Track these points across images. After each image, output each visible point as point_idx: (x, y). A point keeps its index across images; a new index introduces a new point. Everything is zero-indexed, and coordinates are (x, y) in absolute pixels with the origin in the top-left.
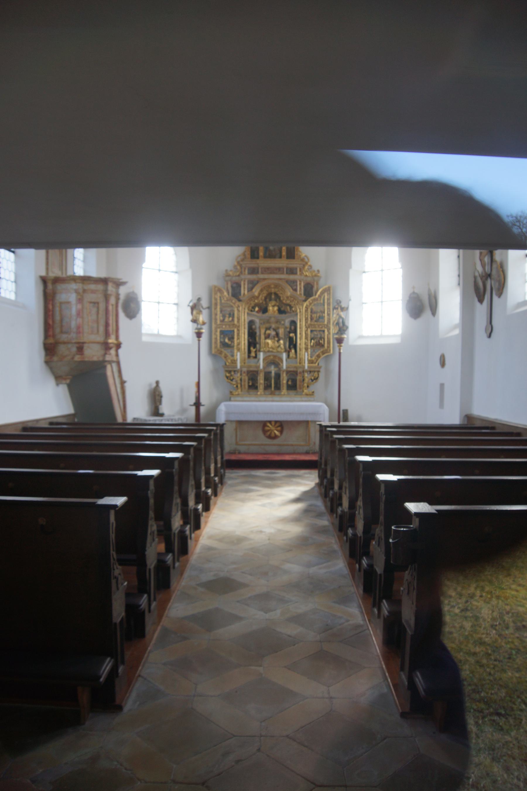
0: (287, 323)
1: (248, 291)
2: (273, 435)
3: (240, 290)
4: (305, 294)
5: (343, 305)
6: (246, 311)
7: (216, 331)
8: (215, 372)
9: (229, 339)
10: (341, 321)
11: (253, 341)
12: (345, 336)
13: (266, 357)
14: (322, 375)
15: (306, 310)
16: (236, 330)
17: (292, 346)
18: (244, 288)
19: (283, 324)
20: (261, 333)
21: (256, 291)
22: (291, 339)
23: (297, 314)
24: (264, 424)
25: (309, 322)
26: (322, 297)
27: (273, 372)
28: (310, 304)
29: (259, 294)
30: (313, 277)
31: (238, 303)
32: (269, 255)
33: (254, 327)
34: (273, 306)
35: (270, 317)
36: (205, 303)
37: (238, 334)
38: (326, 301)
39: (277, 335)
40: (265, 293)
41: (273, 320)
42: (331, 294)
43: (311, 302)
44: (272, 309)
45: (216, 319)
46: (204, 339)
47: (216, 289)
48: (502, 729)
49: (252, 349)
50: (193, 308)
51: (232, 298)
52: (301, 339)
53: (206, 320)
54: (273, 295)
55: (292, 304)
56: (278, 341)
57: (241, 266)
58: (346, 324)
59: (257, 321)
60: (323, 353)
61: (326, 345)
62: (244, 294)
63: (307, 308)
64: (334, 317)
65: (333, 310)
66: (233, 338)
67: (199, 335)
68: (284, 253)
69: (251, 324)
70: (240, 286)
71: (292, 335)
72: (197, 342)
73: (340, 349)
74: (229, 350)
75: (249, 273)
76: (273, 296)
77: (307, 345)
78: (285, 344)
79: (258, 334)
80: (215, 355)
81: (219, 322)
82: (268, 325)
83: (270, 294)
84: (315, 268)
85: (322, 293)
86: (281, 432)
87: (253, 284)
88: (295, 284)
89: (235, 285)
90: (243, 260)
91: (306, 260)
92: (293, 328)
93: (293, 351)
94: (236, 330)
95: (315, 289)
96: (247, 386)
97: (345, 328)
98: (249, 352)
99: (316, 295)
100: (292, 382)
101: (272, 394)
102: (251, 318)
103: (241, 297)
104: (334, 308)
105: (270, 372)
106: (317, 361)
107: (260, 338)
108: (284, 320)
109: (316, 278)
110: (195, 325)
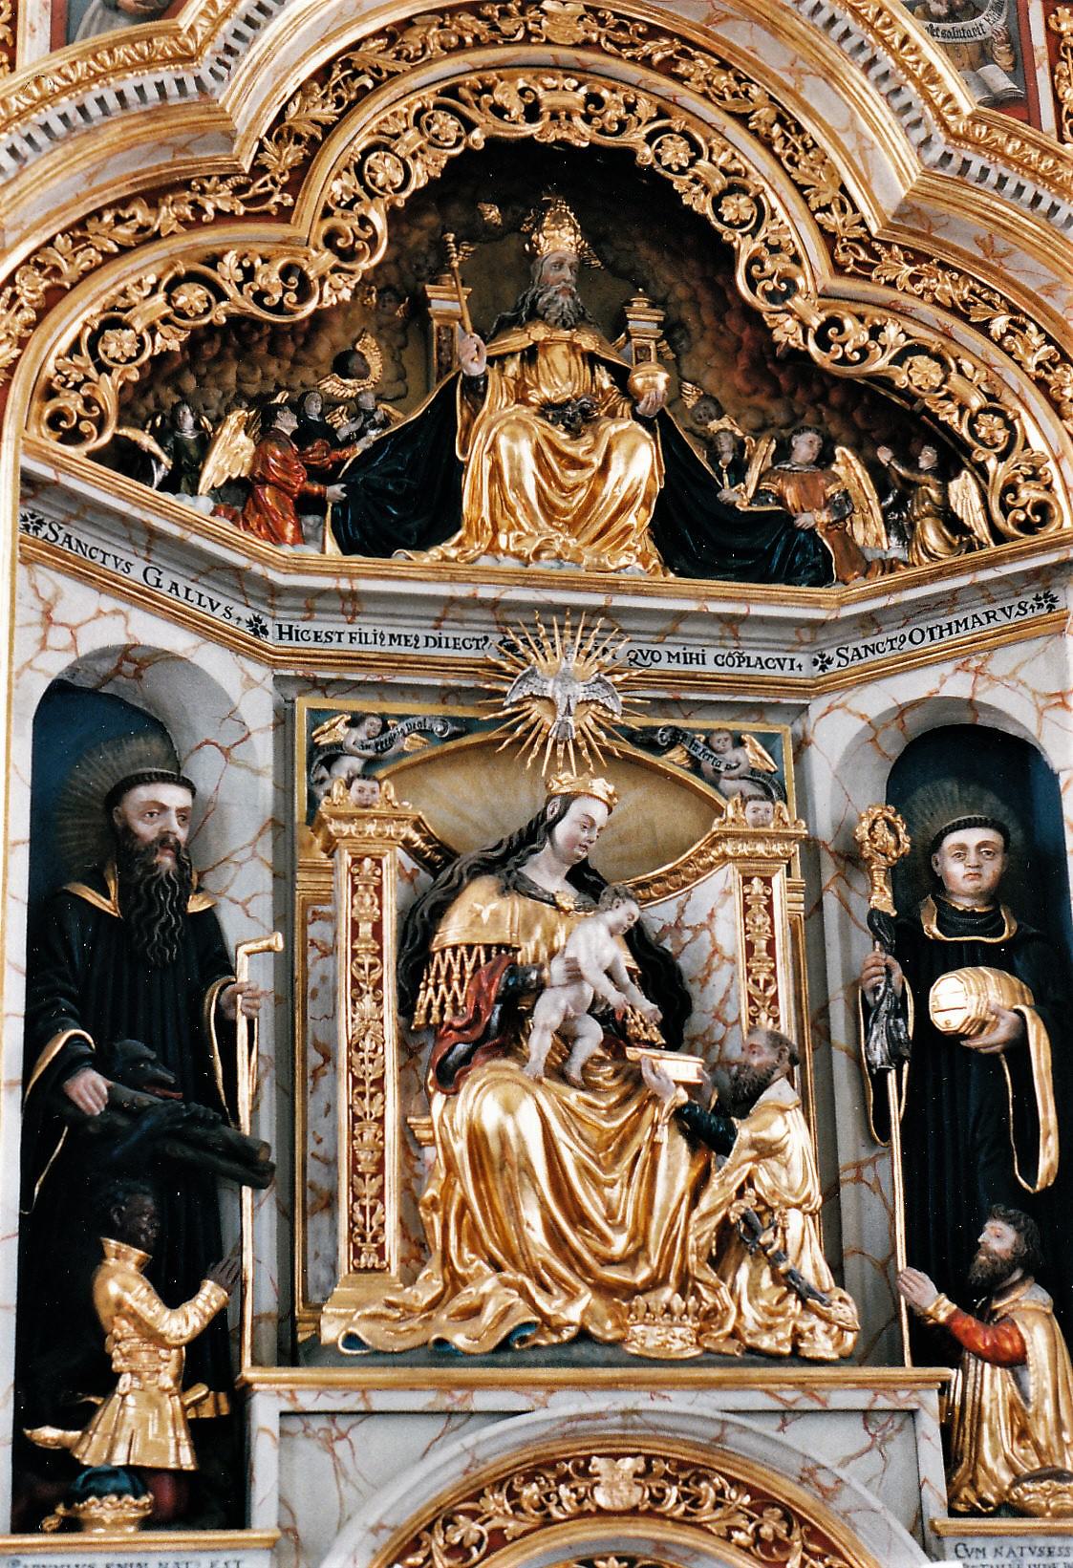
41: (566, 684)
44: (561, 473)
49: (122, 1281)
56: (708, 1128)
59: (233, 692)
82: (468, 803)
102: (97, 624)
107: (296, 1066)
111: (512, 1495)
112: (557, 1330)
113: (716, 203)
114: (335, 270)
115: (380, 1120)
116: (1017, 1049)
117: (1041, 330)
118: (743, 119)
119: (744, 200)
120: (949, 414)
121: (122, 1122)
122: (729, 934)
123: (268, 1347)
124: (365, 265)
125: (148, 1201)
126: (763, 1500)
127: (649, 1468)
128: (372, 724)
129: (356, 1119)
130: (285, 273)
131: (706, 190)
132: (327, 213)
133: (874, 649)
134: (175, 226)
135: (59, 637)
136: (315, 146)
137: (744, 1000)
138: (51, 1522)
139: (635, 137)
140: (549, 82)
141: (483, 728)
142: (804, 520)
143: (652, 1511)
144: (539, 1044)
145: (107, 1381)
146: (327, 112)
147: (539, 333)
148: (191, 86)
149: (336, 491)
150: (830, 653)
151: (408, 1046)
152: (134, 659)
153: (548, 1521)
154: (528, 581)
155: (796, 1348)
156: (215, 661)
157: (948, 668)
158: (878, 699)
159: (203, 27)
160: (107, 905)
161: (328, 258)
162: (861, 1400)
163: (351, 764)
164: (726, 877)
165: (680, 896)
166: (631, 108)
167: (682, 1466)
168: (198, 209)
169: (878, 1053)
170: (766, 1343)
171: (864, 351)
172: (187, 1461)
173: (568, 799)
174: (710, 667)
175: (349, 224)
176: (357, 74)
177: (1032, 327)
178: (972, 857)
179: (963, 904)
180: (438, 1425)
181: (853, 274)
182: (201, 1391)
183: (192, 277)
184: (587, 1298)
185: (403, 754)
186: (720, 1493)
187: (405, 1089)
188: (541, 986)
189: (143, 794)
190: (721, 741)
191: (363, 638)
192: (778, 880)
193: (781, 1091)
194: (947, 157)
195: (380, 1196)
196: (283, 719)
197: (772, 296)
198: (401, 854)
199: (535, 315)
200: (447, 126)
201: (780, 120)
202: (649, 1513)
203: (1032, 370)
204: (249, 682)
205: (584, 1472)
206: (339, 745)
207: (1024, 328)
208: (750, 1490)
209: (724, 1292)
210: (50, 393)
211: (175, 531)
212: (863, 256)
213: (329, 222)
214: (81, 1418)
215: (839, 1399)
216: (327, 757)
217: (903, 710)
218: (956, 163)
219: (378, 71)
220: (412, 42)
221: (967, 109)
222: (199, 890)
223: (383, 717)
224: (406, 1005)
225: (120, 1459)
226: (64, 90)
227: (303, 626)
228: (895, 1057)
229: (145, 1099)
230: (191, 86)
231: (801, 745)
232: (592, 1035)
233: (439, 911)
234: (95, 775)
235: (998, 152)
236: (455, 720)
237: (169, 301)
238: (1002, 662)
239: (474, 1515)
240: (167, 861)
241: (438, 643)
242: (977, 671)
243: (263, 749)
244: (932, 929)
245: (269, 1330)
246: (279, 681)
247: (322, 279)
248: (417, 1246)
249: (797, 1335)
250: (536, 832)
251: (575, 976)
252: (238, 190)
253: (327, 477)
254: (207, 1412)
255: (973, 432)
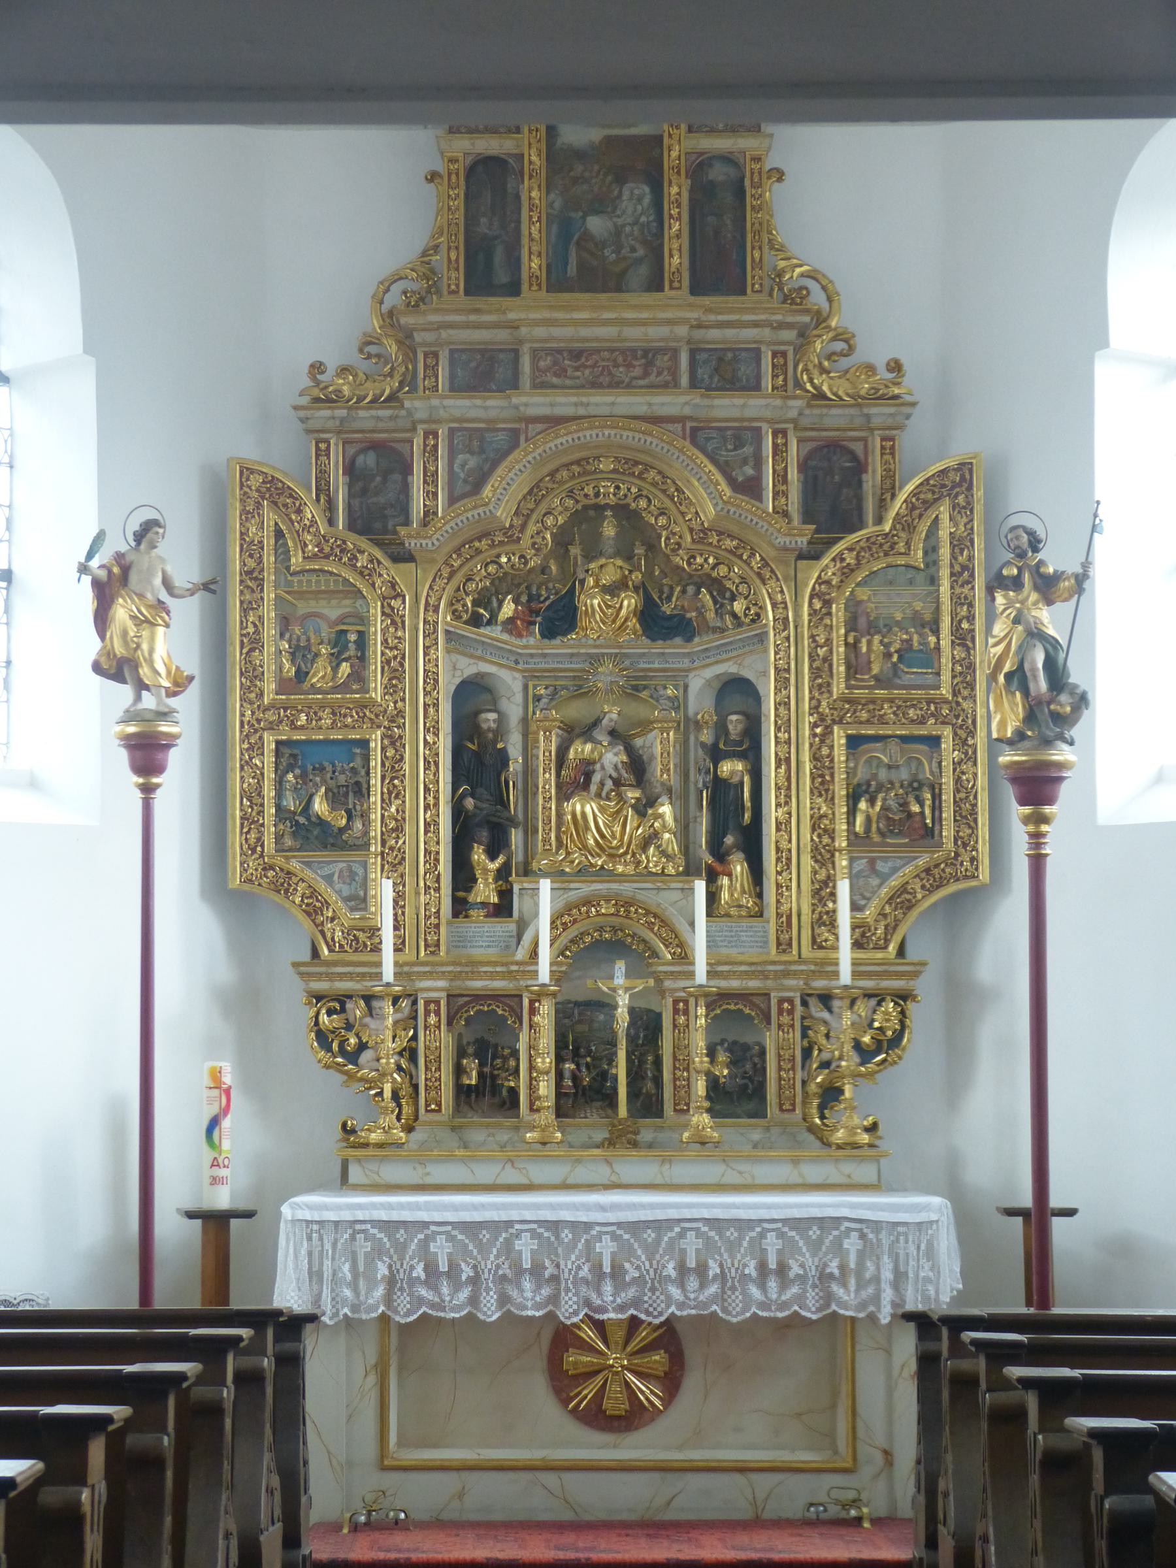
1: (452, 500)
2: (615, 1403)
3: (406, 488)
4: (808, 516)
5: (1054, 559)
6: (444, 617)
7: (256, 748)
8: (242, 1004)
9: (335, 798)
10: (1039, 657)
11: (485, 808)
12: (1062, 753)
13: (568, 909)
14: (925, 1016)
15: (820, 616)
16: (376, 740)
17: (729, 840)
19: (678, 704)
20: (530, 752)
21: (502, 496)
22: (722, 796)
23: (762, 638)
24: (560, 1349)
25: (838, 687)
26: (923, 528)
27: (623, 1001)
28: (847, 572)
29: (523, 515)
30: (859, 401)
31: (390, 570)
32: (585, 271)
33: (489, 719)
34: (612, 590)
36: (180, 557)
37: (393, 770)
38: (945, 552)
39: (638, 767)
41: (606, 675)
42: (978, 509)
43: (850, 559)
44: (606, 609)
45: (252, 674)
46: (182, 772)
47: (255, 481)
49: (478, 855)
50: (106, 593)
51: (353, 541)
53: (191, 664)
54: (607, 520)
56: (644, 808)
57: (406, 340)
58: (1075, 677)
59: (510, 683)
60: (933, 878)
61: (948, 832)
62: (430, 513)
64: (996, 640)
65: (990, 591)
66: (361, 790)
67: (146, 752)
68: (676, 259)
69: (472, 696)
71: (730, 768)
72: (139, 804)
73: (1037, 838)
74: (338, 864)
75: (456, 388)
76: (609, 530)
77: (831, 834)
79: (515, 765)
80: (242, 889)
81: (269, 687)
82: (577, 711)
83: (587, 517)
84: (875, 349)
85: (921, 504)
86: (671, 1383)
87: (484, 451)
88: (748, 450)
89: (369, 460)
90: (417, 302)
91: (818, 298)
92: (735, 723)
93: (739, 868)
94: (376, 740)
95: (871, 481)
96: (447, 1094)
97: (1064, 703)
98: (463, 875)
99: (879, 520)
100: (732, 1064)
101: (621, 1139)
102: (469, 668)
104: (998, 582)
106: (890, 930)
108: (680, 678)
109: (880, 413)
110: (123, 693)
113: (656, 519)
122: (658, 749)
123: (521, 871)
124: (545, 551)
128: (551, 689)
130: (520, 558)
135: (458, 673)
139: (629, 500)
141: (581, 690)
142: (688, 615)
143: (616, 915)
144: (593, 788)
145: (475, 880)
146: (531, 506)
147: (603, 561)
149: (539, 619)
151: (559, 787)
152: (481, 675)
154: (596, 647)
156: (505, 675)
158: (709, 673)
159: (490, 495)
162: (680, 885)
166: (629, 490)
168: (493, 541)
169: (700, 785)
171: (702, 566)
172: (496, 900)
173: (606, 713)
175: (539, 540)
179: (733, 737)
183: (492, 562)
188: (594, 771)
192: (671, 734)
196: (526, 687)
199: (601, 554)
200: (570, 503)
204: (515, 678)
210: (453, 604)
214: (468, 890)
215: (673, 885)
216: (538, 699)
217: (718, 676)
220: (558, 477)
224: (558, 775)
228: (705, 786)
229: (484, 806)
232: (609, 784)
233: (567, 749)
238: (748, 661)
240: (491, 735)
243: (519, 698)
244: (721, 746)
249: (663, 868)
250: (596, 723)
251: (603, 768)
253: (537, 613)
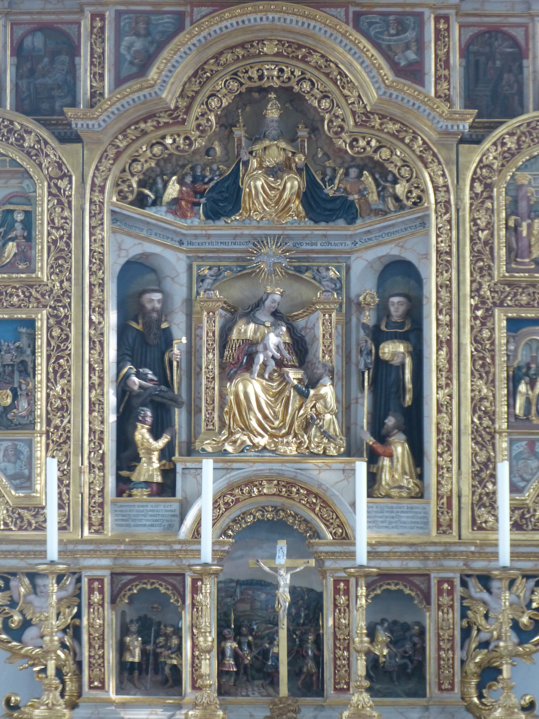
0: (363, 283)
3: (72, 71)
4: (470, 101)
13: (231, 489)
17: (390, 421)
18: (97, 60)
19: (340, 285)
20: (192, 337)
21: (168, 78)
22: (384, 377)
23: (424, 222)
25: (500, 269)
27: (285, 580)
28: (508, 156)
29: (189, 98)
31: (56, 150)
35: (259, 241)
37: (58, 350)
39: (299, 348)
40: (224, 92)
41: (269, 257)
44: (269, 191)
48: (420, 198)
49: (142, 434)
51: (21, 121)
52: (447, 373)
55: (394, 156)
59: (175, 263)
62: (96, 95)
63: (485, 184)
69: (137, 275)
70: (74, 51)
71: (393, 350)
76: (273, 113)
77: (492, 416)
78: (346, 409)
82: (239, 291)
83: (252, 98)
88: (410, 35)
89: (38, 41)
92: (397, 305)
93: (400, 449)
94: (42, 319)
98: (128, 454)
100: (393, 643)
102: (134, 248)
103: (76, 117)
105: (268, 585)
111: (242, 490)
112: (258, 447)
113: (319, 102)
114: (200, 137)
115: (214, 388)
116: (403, 365)
117: (422, 139)
118: (327, 75)
119: (328, 100)
120: (391, 167)
121: (142, 391)
123: (184, 450)
125: (149, 413)
126: (309, 493)
127: (278, 483)
128: (215, 269)
129: (207, 388)
131: (316, 98)
132: (197, 119)
133: (370, 239)
134: (152, 128)
135: (123, 253)
136: (193, 98)
137: (321, 351)
138: (124, 495)
140: (267, 67)
144: (257, 368)
146: (196, 88)
147: (267, 143)
148: (153, 95)
149: (203, 200)
150: (357, 240)
151: (222, 367)
152: (146, 255)
153: (251, 497)
154: (259, 228)
155: (324, 452)
157: (392, 245)
160: (139, 327)
161: (198, 133)
163: (208, 281)
164: (319, 314)
165: (306, 318)
166: (292, 73)
167: (288, 483)
170: (315, 451)
171: (364, 149)
174: (319, 247)
175: (203, 122)
176: (205, 73)
177: (419, 138)
178: (396, 306)
180: (225, 471)
181: (361, 125)
182: (164, 462)
184: (267, 437)
185: (225, 277)
186: (298, 490)
187: (221, 379)
189: (147, 296)
190: (322, 270)
191: (212, 243)
192: (334, 315)
193: (327, 380)
194: (385, 93)
195: (213, 410)
196: (190, 268)
197: (336, 133)
198: (220, 310)
199: (265, 136)
200: (234, 85)
201: (340, 73)
202: (278, 495)
203: (418, 153)
204: (179, 259)
205: (261, 484)
206: (205, 276)
207: (417, 139)
208: (307, 490)
209: (306, 437)
210: (118, 185)
211: (154, 222)
212: (364, 119)
213: (198, 122)
214: (132, 469)
216: (202, 279)
217: (380, 258)
218: (388, 94)
219: (212, 71)
220: (223, 60)
221: (391, 78)
222: (166, 321)
223: (219, 267)
224: (221, 355)
225: (142, 479)
226: (117, 101)
227: (195, 241)
230: (153, 95)
231: (348, 269)
232: (272, 364)
233: (230, 329)
234: (135, 288)
235: (402, 91)
236: (240, 266)
237: (151, 152)
239: (231, 495)
240: (155, 315)
241: (235, 244)
242: (402, 247)
243: (183, 278)
245: (184, 446)
246: (188, 257)
247: (196, 140)
248: (223, 425)
249: (325, 449)
250: (259, 304)
252: (170, 115)
254: (167, 467)
255: (399, 173)
